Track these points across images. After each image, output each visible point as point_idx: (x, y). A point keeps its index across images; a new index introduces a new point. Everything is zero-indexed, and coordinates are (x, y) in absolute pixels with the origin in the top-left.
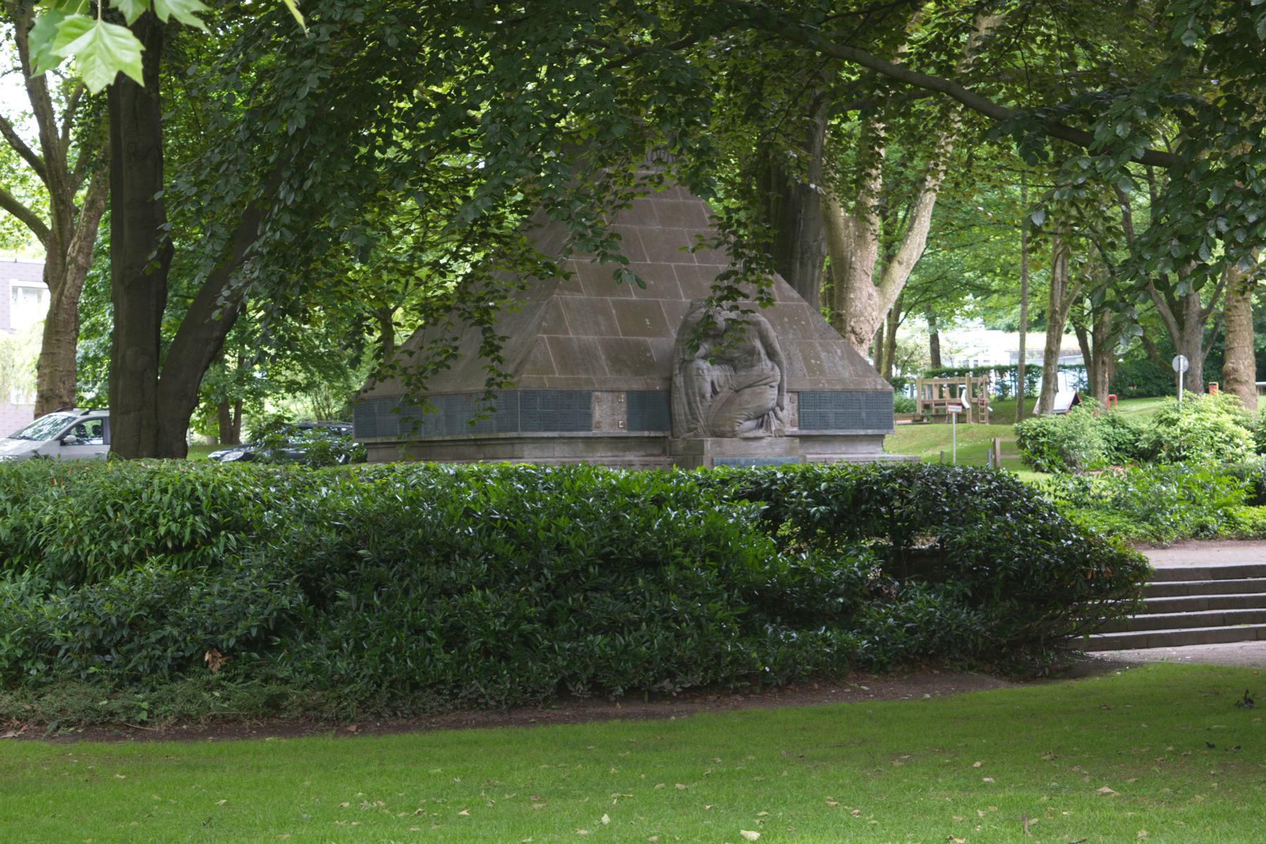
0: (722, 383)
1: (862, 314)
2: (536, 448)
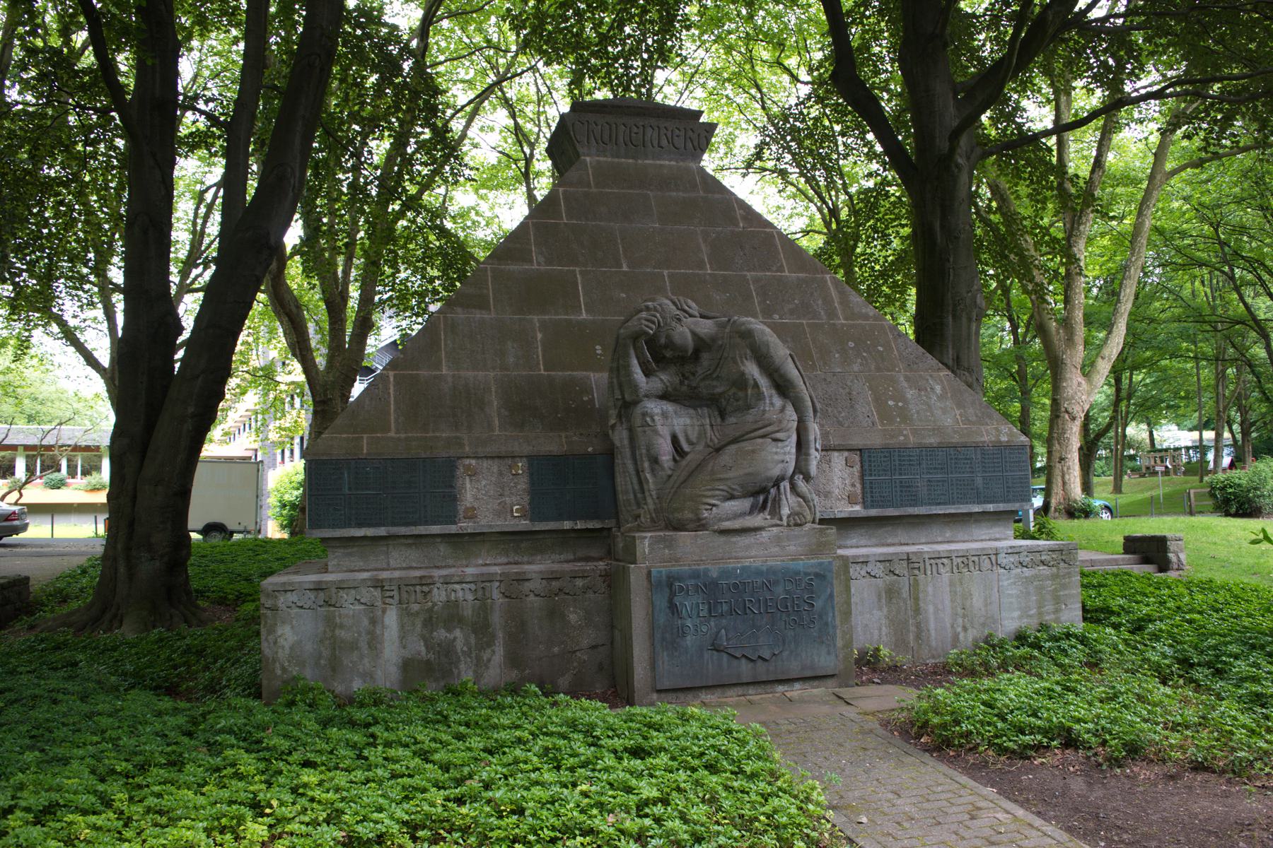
0: (693, 437)
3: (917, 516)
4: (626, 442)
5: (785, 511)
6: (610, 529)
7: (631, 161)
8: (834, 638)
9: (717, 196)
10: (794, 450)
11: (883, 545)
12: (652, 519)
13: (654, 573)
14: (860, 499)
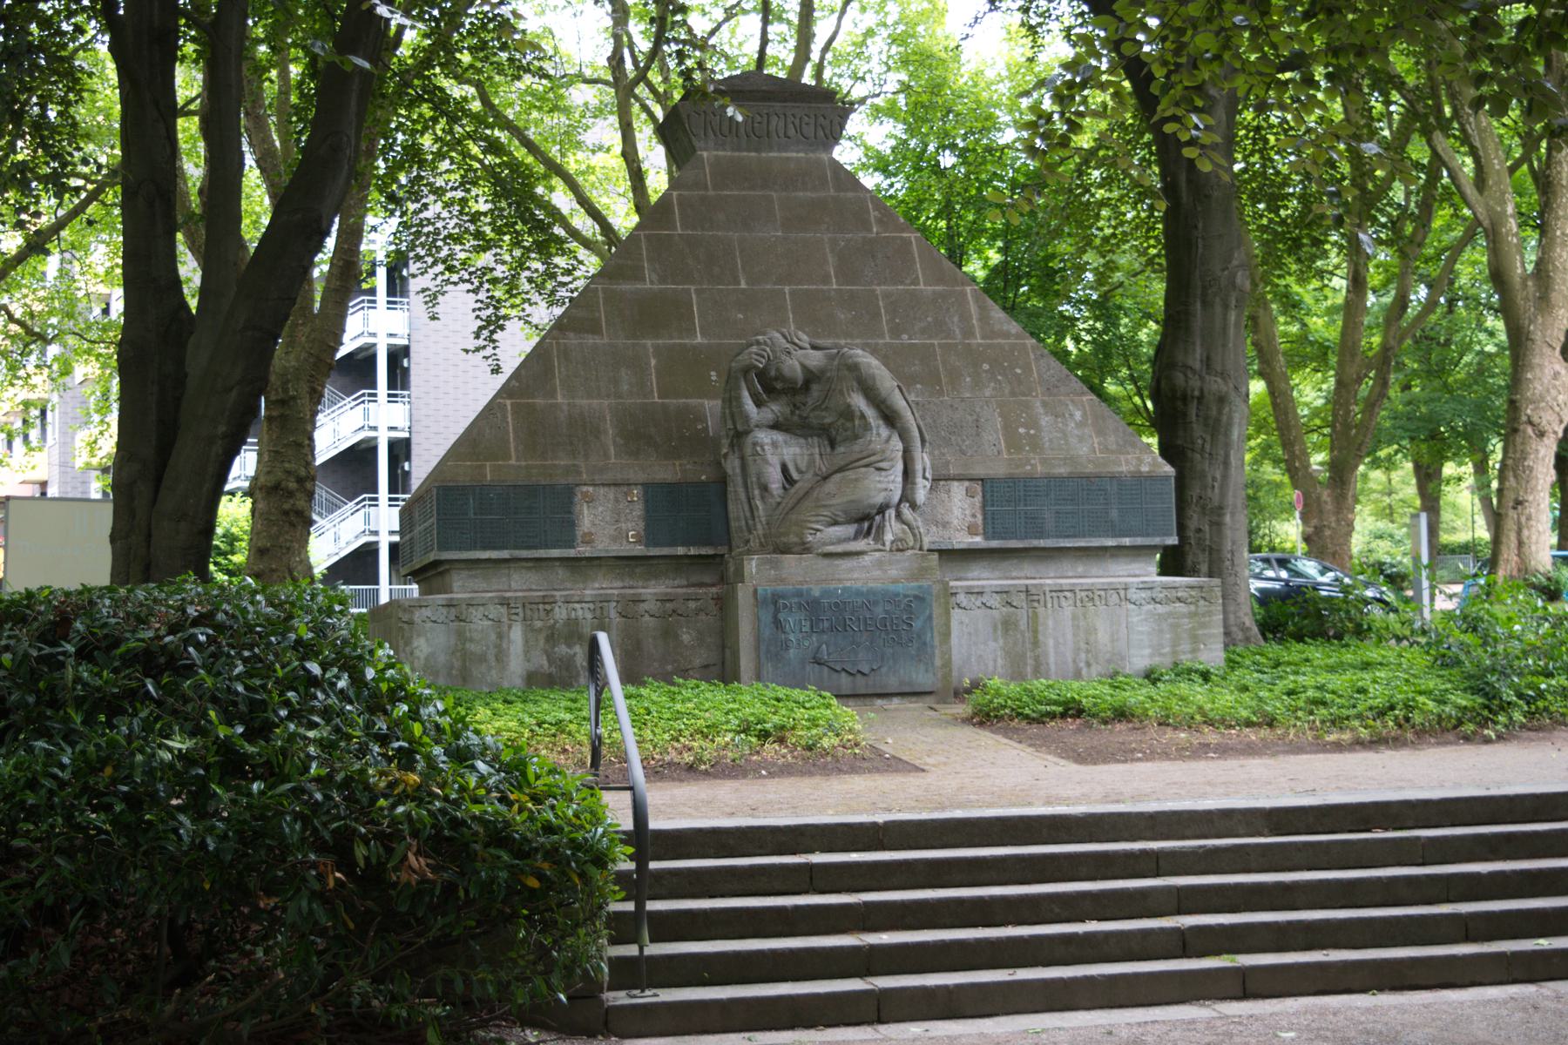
0: (803, 466)
1: (1542, 398)
2: (475, 577)
3: (1044, 549)
4: (738, 471)
5: (889, 537)
6: (722, 556)
7: (753, 154)
8: (933, 656)
9: (850, 195)
10: (900, 479)
11: (1007, 578)
12: (761, 543)
13: (760, 590)
14: (981, 530)
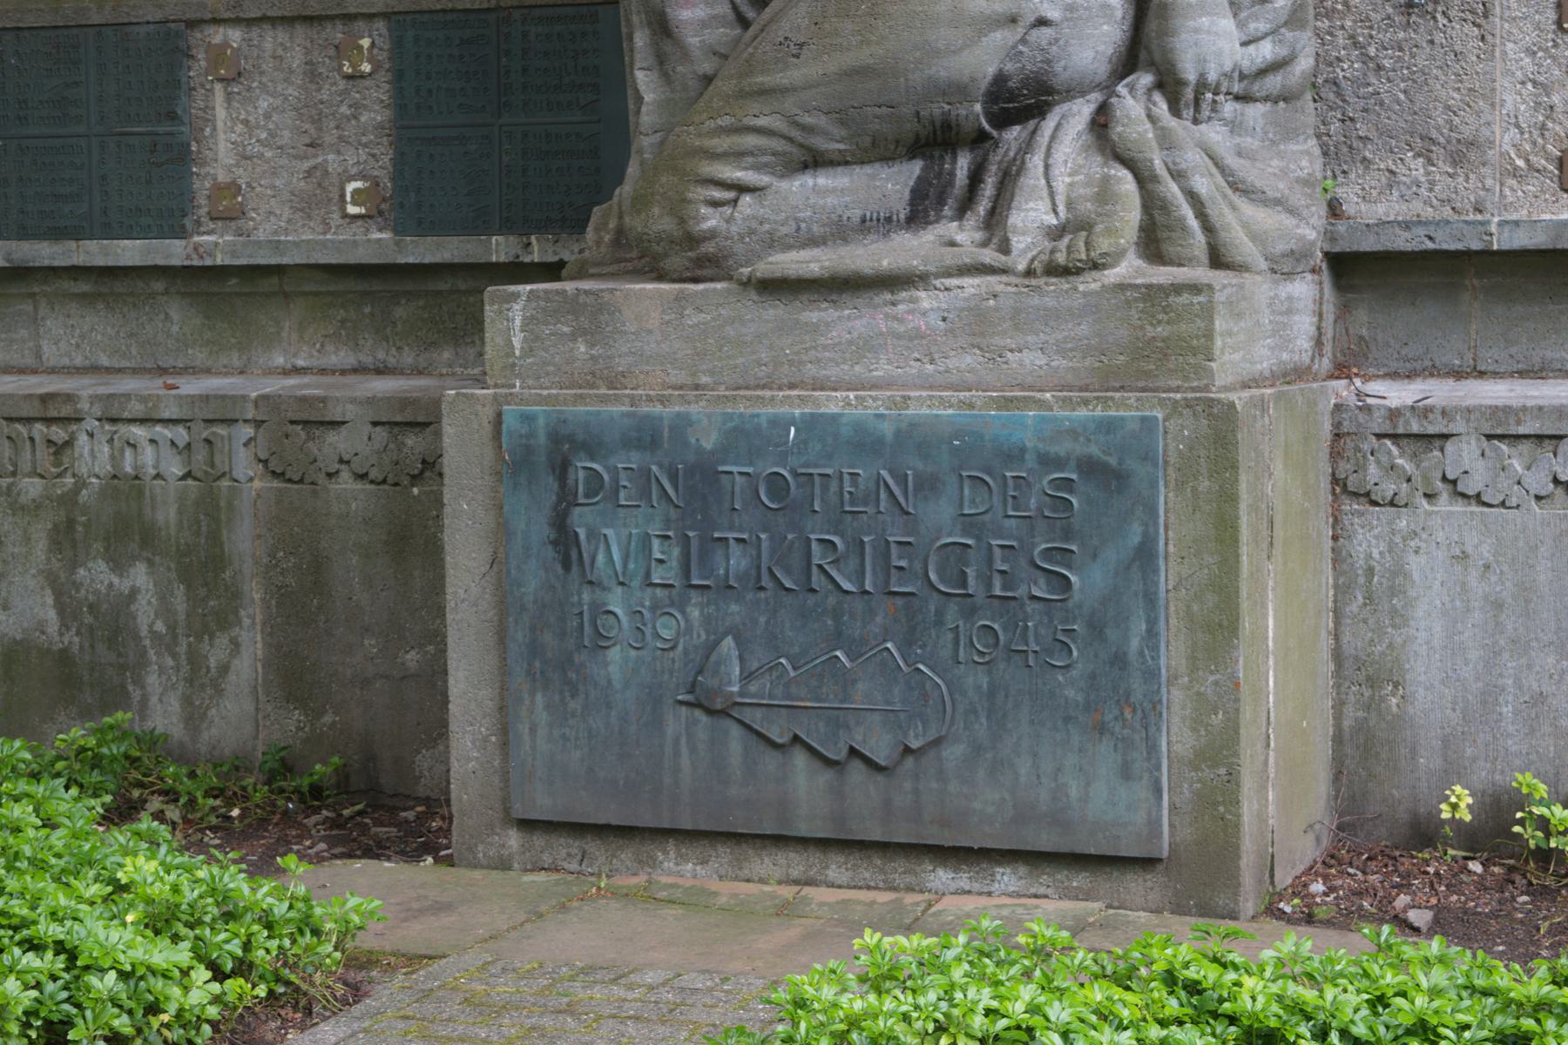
8: (1151, 713)
13: (510, 422)
